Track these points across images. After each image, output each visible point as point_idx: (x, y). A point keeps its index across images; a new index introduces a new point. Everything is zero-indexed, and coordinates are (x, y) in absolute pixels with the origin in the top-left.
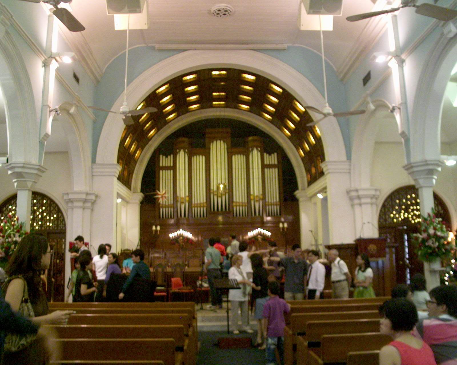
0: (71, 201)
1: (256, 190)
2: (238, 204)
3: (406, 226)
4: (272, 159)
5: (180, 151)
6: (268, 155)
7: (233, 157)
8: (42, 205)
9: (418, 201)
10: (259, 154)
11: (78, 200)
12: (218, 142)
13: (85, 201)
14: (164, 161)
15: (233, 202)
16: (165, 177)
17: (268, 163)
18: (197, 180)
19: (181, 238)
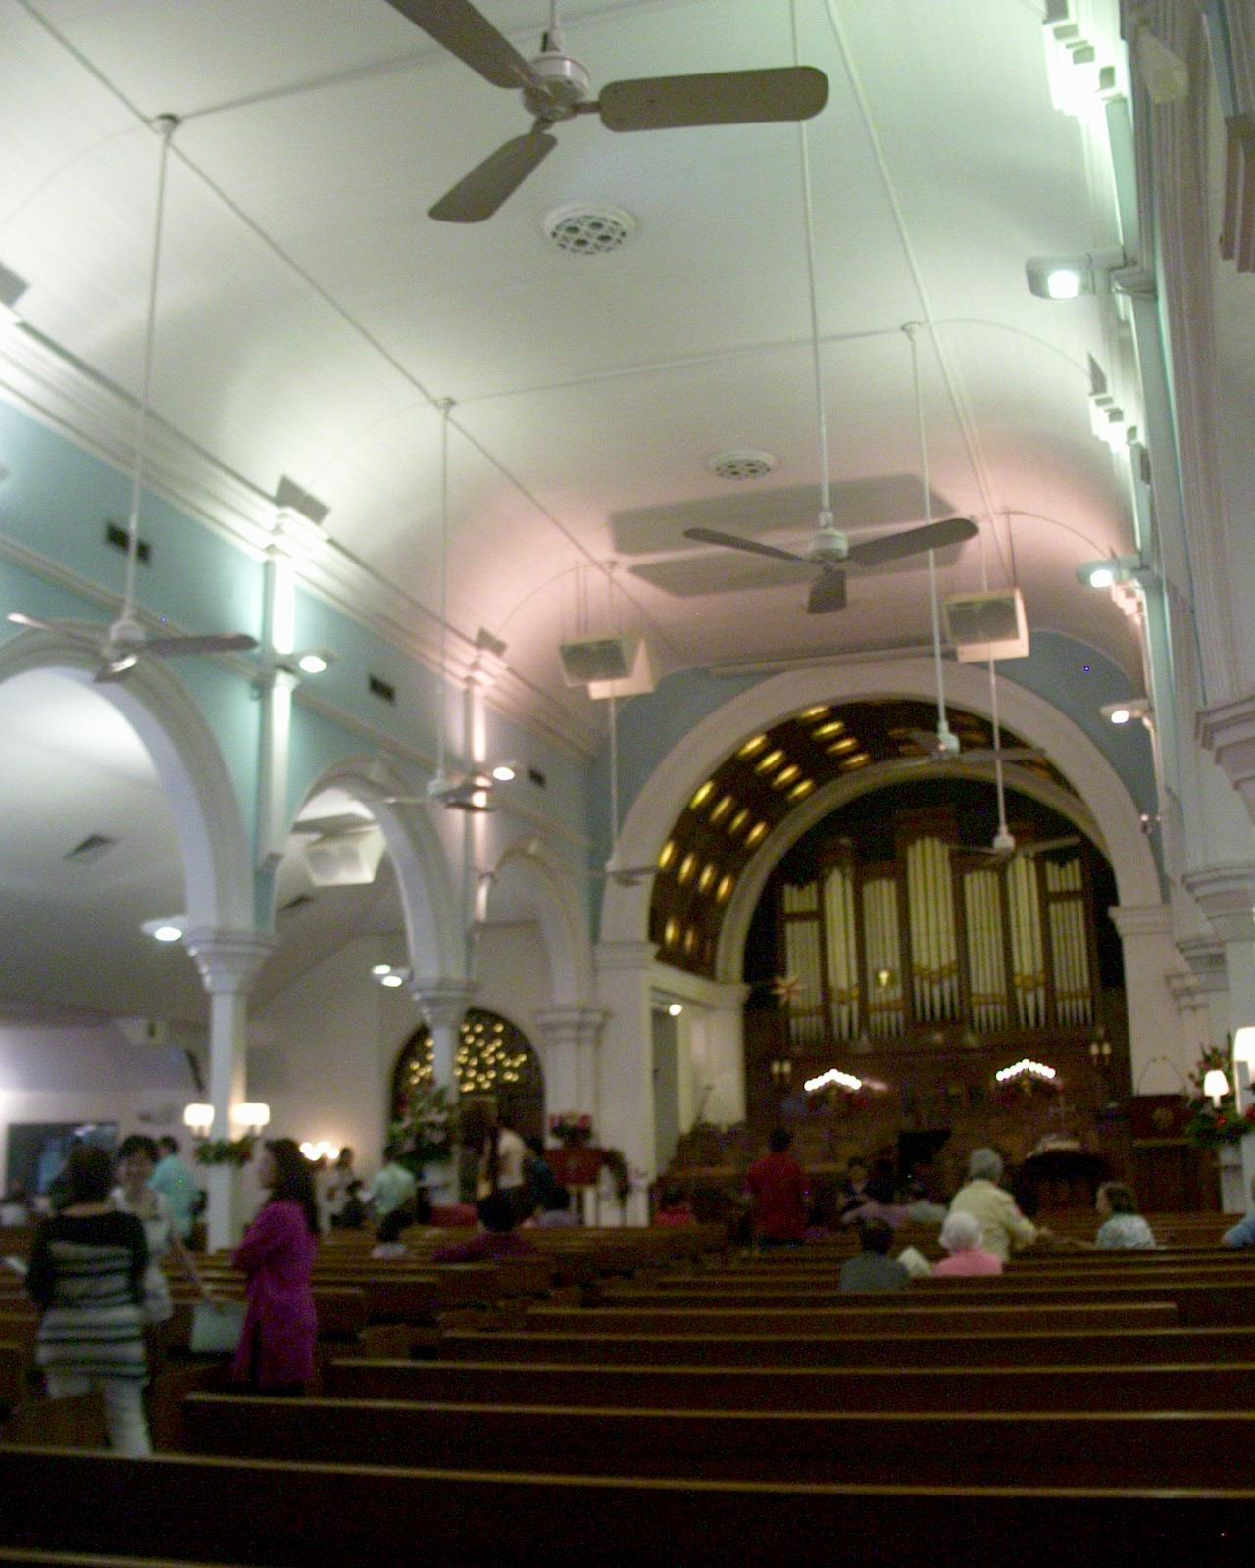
0: (549, 1027)
1: (1027, 960)
2: (982, 999)
3: (1113, 1047)
4: (1069, 876)
5: (831, 872)
6: (1056, 867)
7: (967, 878)
8: (494, 1036)
9: (459, 1073)
10: (1032, 867)
11: (562, 1025)
12: (928, 842)
13: (580, 1026)
14: (795, 899)
15: (970, 994)
16: (798, 939)
17: (1058, 889)
18: (906, 935)
19: (834, 1092)
